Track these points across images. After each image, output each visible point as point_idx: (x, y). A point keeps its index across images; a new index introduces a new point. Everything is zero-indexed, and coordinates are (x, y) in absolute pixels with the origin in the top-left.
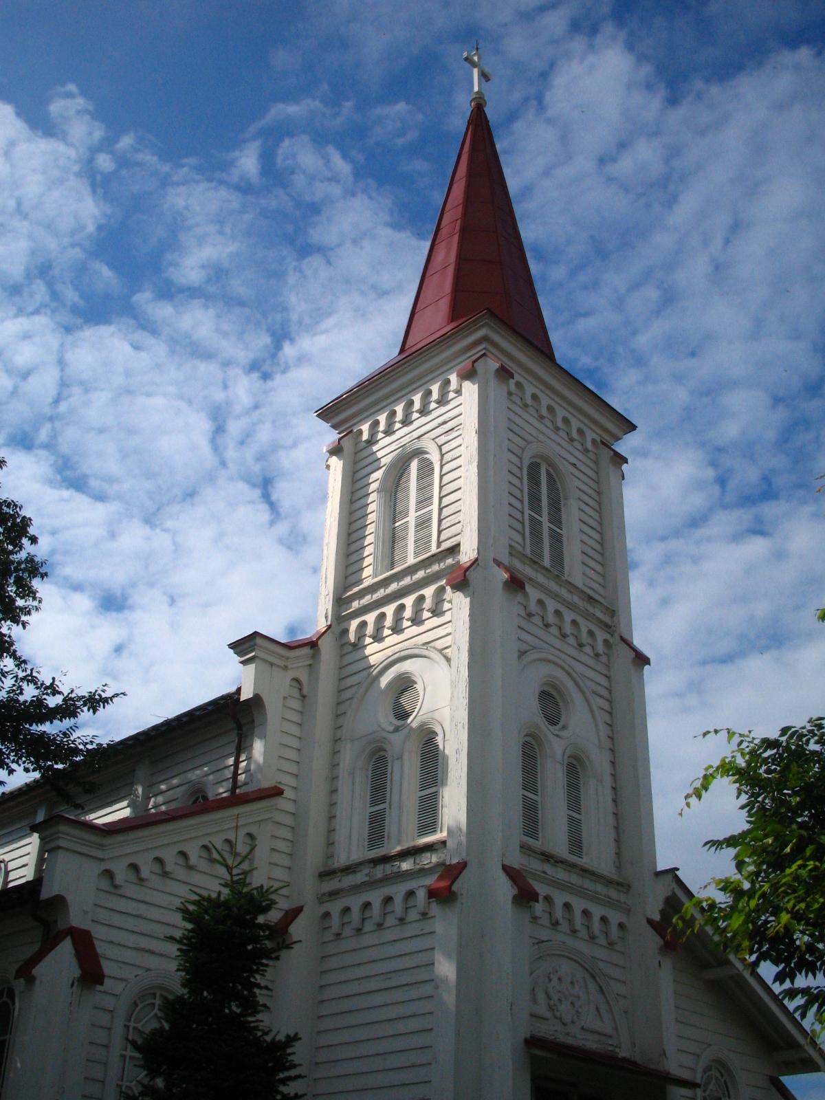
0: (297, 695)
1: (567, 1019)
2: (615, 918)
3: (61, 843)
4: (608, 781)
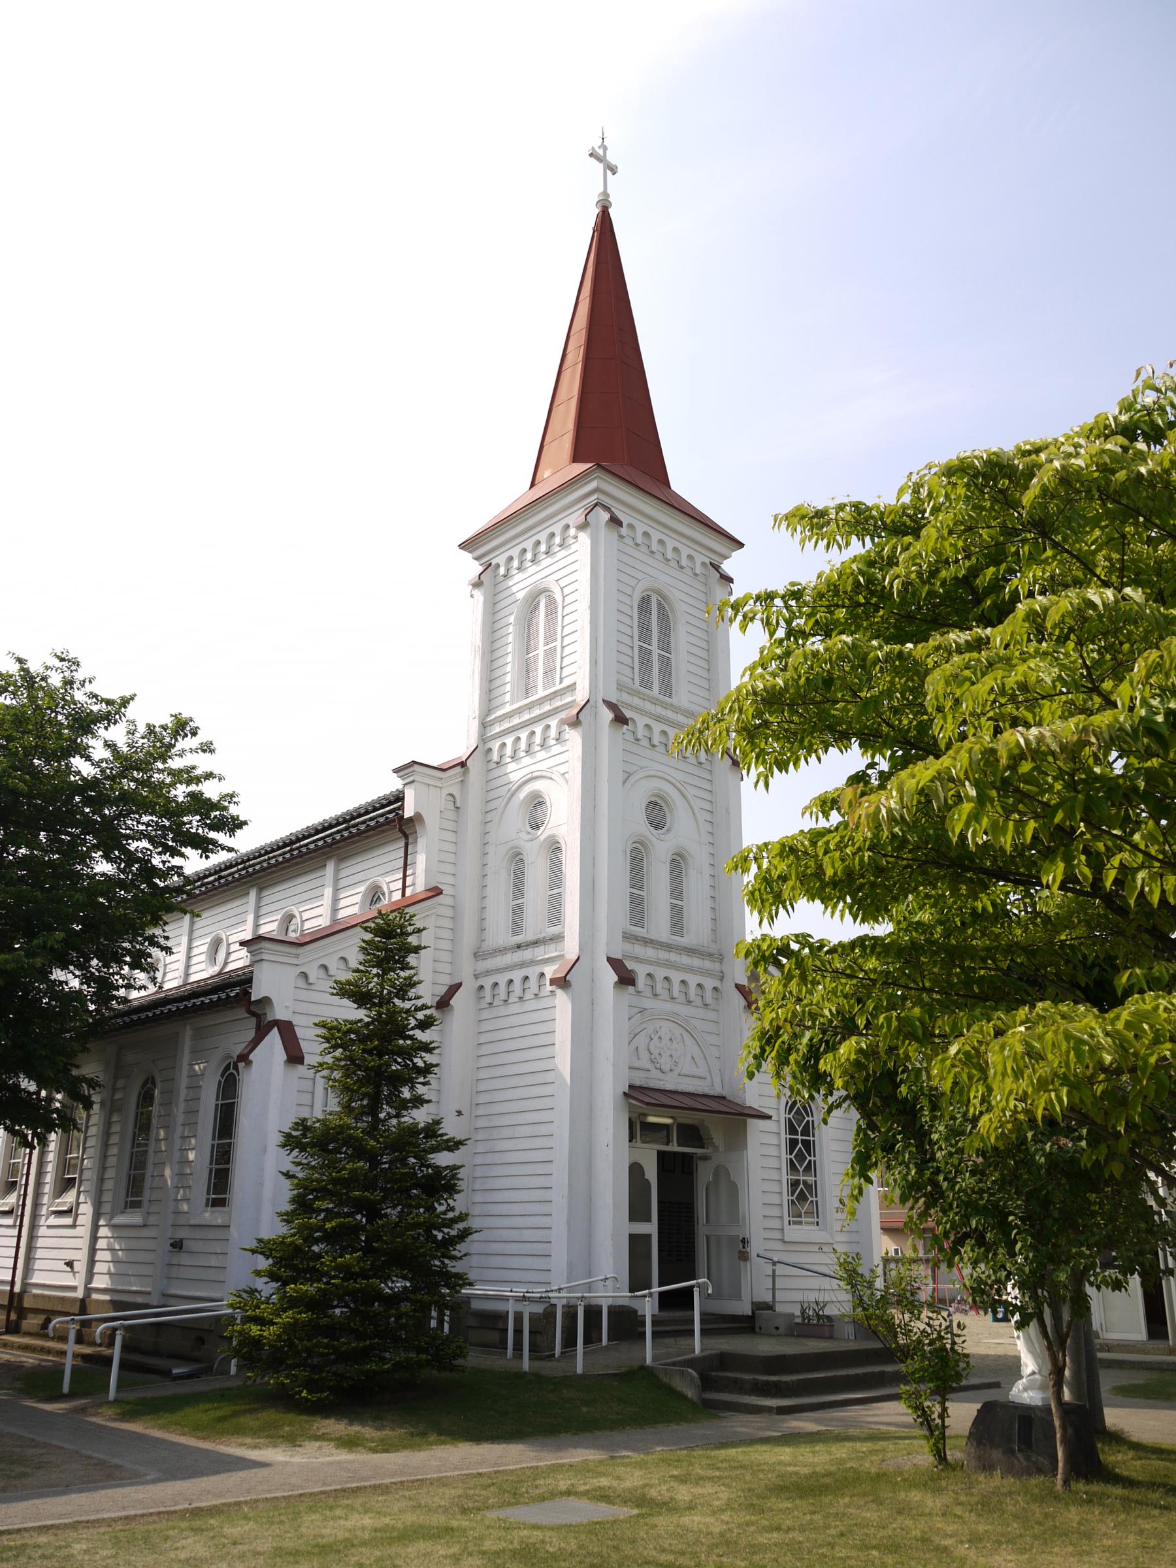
0: (452, 807)
1: (666, 1068)
2: (709, 984)
3: (264, 957)
4: (707, 871)
